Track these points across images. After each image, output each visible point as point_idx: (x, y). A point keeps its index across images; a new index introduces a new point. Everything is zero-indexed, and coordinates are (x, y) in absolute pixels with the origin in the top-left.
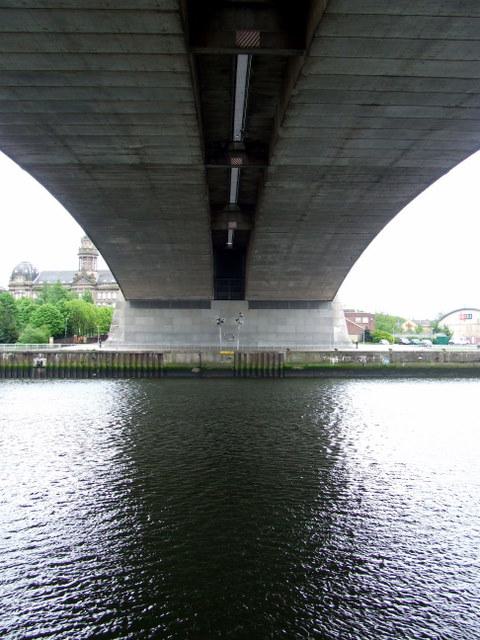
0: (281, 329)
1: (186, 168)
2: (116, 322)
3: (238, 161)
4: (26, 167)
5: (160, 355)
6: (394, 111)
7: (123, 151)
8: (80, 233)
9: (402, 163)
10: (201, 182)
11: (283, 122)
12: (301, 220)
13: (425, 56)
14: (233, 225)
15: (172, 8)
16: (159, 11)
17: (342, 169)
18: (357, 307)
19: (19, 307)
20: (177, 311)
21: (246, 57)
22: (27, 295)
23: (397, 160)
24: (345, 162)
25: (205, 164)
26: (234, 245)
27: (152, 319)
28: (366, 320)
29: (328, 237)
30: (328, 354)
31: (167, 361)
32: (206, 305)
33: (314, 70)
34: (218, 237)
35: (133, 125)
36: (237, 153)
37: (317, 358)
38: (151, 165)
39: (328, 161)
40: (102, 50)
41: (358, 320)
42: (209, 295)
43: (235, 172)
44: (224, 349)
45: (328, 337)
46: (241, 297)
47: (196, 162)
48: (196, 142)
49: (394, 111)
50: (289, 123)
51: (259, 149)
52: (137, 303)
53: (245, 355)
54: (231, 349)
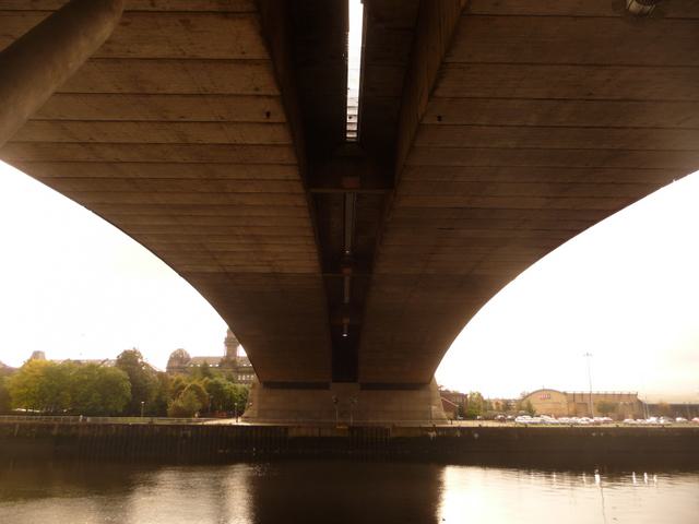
3: (347, 271)
4: (182, 274)
5: (286, 428)
8: (225, 327)
10: (265, 136)
14: (346, 321)
19: (12, 393)
22: (181, 376)
30: (427, 429)
31: (293, 433)
32: (326, 386)
37: (419, 433)
43: (347, 279)
44: (340, 424)
45: (427, 414)
46: (355, 381)
51: (365, 260)
54: (345, 424)
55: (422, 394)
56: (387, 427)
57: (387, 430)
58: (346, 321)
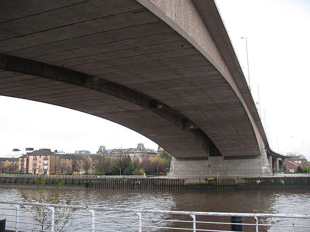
0: (238, 168)
2: (172, 167)
5: (183, 180)
20: (194, 161)
27: (184, 165)
31: (186, 182)
41: (296, 162)
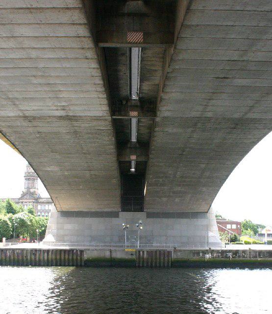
1: (97, 119)
5: (82, 251)
6: (240, 82)
7: (55, 108)
8: (25, 162)
9: (250, 116)
11: (163, 88)
12: (182, 154)
13: (254, 49)
15: (82, 22)
16: (74, 24)
17: (210, 119)
18: (228, 217)
21: (137, 49)
23: (246, 113)
24: (209, 115)
25: (112, 116)
26: (136, 171)
28: (234, 227)
29: (203, 166)
30: (205, 252)
31: (86, 256)
32: (115, 215)
33: (181, 57)
34: (123, 167)
35: (60, 91)
36: (134, 108)
38: (74, 116)
39: (197, 114)
40: (38, 46)
41: (229, 226)
42: (117, 208)
45: (204, 240)
46: (141, 210)
47: (105, 114)
48: (105, 102)
49: (240, 82)
50: (168, 90)
52: (65, 214)
53: (143, 252)
55: (200, 222)
56: (168, 249)
57: (169, 253)
58: (133, 157)
